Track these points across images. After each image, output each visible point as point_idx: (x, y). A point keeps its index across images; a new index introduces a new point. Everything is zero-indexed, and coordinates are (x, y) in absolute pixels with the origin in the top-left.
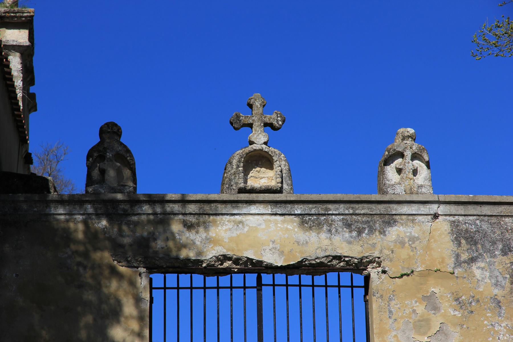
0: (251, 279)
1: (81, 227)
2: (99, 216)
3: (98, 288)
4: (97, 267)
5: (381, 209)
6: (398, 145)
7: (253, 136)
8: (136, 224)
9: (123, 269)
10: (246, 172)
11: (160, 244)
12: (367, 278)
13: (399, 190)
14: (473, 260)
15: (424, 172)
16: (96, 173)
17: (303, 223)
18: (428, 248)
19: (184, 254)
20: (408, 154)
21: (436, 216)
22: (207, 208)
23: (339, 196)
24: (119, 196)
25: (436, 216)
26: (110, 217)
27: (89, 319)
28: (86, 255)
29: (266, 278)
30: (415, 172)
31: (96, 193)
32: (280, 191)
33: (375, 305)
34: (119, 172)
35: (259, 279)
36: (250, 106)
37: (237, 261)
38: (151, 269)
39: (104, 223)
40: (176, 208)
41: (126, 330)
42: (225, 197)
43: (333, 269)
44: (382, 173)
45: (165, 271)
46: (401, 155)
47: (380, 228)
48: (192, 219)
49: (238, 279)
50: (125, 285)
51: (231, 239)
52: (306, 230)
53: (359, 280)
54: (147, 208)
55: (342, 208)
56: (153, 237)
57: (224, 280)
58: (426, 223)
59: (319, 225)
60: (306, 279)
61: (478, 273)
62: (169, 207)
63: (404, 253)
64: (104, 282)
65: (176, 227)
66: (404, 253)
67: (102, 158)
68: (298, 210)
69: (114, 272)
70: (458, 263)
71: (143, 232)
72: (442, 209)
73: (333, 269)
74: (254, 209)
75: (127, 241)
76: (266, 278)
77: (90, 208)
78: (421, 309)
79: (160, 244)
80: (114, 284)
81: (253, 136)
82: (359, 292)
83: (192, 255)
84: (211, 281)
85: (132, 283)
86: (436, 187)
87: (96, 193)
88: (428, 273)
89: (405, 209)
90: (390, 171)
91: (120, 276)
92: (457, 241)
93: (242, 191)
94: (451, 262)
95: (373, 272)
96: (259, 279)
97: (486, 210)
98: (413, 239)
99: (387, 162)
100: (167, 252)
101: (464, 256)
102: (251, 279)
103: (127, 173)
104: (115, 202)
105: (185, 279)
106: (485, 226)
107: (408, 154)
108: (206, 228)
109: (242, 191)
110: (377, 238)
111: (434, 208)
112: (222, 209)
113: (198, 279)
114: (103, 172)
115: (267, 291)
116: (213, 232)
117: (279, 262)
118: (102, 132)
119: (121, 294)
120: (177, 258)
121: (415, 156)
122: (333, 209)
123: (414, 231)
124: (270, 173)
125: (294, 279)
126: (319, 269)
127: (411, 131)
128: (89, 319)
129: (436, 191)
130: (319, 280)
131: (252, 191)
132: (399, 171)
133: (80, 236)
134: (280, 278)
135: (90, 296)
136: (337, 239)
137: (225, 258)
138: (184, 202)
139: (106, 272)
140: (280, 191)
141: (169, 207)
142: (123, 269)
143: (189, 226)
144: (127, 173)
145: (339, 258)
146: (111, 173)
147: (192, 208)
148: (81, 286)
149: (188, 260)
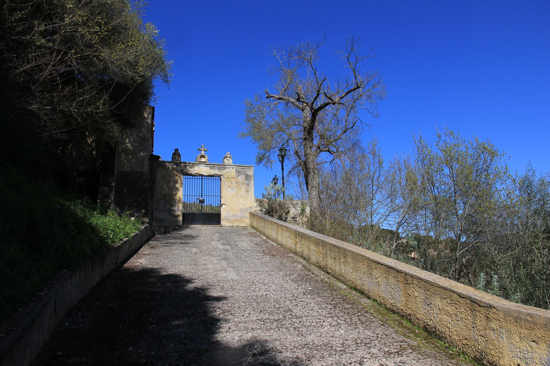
0: (201, 177)
1: (171, 167)
2: (174, 165)
3: (174, 177)
4: (174, 174)
5: (224, 166)
6: (227, 155)
7: (202, 152)
8: (181, 167)
9: (178, 175)
10: (200, 159)
11: (185, 170)
12: (221, 178)
13: (227, 163)
14: (239, 176)
15: (231, 160)
16: (174, 157)
17: (210, 168)
18: (231, 173)
19: (189, 173)
20: (229, 157)
21: (233, 168)
22: (194, 165)
23: (217, 164)
24: (178, 162)
25: (233, 168)
26: (177, 165)
27: (172, 183)
28: (172, 172)
29: (203, 177)
30: (230, 160)
31: (174, 161)
32: (206, 162)
33: (222, 183)
34: (178, 157)
35: (202, 177)
36: (201, 147)
37: (198, 174)
38: (183, 175)
39: (175, 166)
40: (188, 164)
41: (179, 185)
42: (197, 163)
43: (215, 176)
44: (224, 160)
45: (185, 175)
46: (227, 157)
47: (274, 141)
48: (191, 166)
49: (198, 177)
50: (179, 177)
51: (198, 170)
52: (262, 343)
53: (219, 178)
54: (183, 164)
55: (217, 166)
56: (184, 169)
57: (196, 177)
58: (231, 169)
59: (213, 169)
60: (210, 178)
61: (240, 178)
62: (187, 164)
63: (227, 174)
64: (175, 177)
65: (188, 168)
66: (227, 174)
67: (175, 155)
68: (209, 166)
69: (177, 175)
70: (236, 176)
71: (182, 168)
72: (234, 167)
73: (215, 176)
74: (202, 165)
75: (179, 170)
76: (203, 177)
77: (173, 164)
78: (230, 184)
79: (185, 170)
80: (177, 177)
81: (202, 152)
82: (219, 180)
83: (191, 173)
84: (194, 177)
85: (180, 177)
86: (233, 163)
87: (174, 161)
88: (231, 178)
89: (228, 166)
90: (225, 160)
91: (178, 176)
92: (236, 172)
93: (200, 162)
94: (235, 176)
95: (222, 177)
96: (202, 177)
97: (241, 167)
98: (229, 172)
99: (225, 158)
100: (186, 172)
101: (237, 175)
102: (201, 177)
103: (179, 157)
104: (177, 163)
105: (189, 177)
106: (241, 170)
107: (229, 157)
108: (193, 168)
109: (200, 162)
110: (223, 171)
111: (233, 167)
112: (196, 165)
113: (191, 177)
114: (175, 157)
115: (203, 179)
116: (194, 169)
117: (206, 175)
118: (175, 150)
119: (178, 179)
120: (188, 173)
121: (230, 157)
122: (215, 166)
123: (229, 170)
124: (204, 159)
125: (208, 178)
126: (345, 253)
127: (229, 153)
128: (172, 183)
129: (233, 163)
130: (212, 178)
131: (202, 162)
132: (227, 160)
133: (171, 168)
134: (206, 177)
135: (172, 179)
136: (216, 171)
137: (197, 173)
138: (189, 163)
139: (175, 175)
140: (206, 162)
141: (187, 164)
142: (178, 175)
143: (190, 168)
144: (179, 157)
145: (216, 174)
146: (177, 157)
147: (191, 164)
148: (171, 177)
149: (190, 174)
